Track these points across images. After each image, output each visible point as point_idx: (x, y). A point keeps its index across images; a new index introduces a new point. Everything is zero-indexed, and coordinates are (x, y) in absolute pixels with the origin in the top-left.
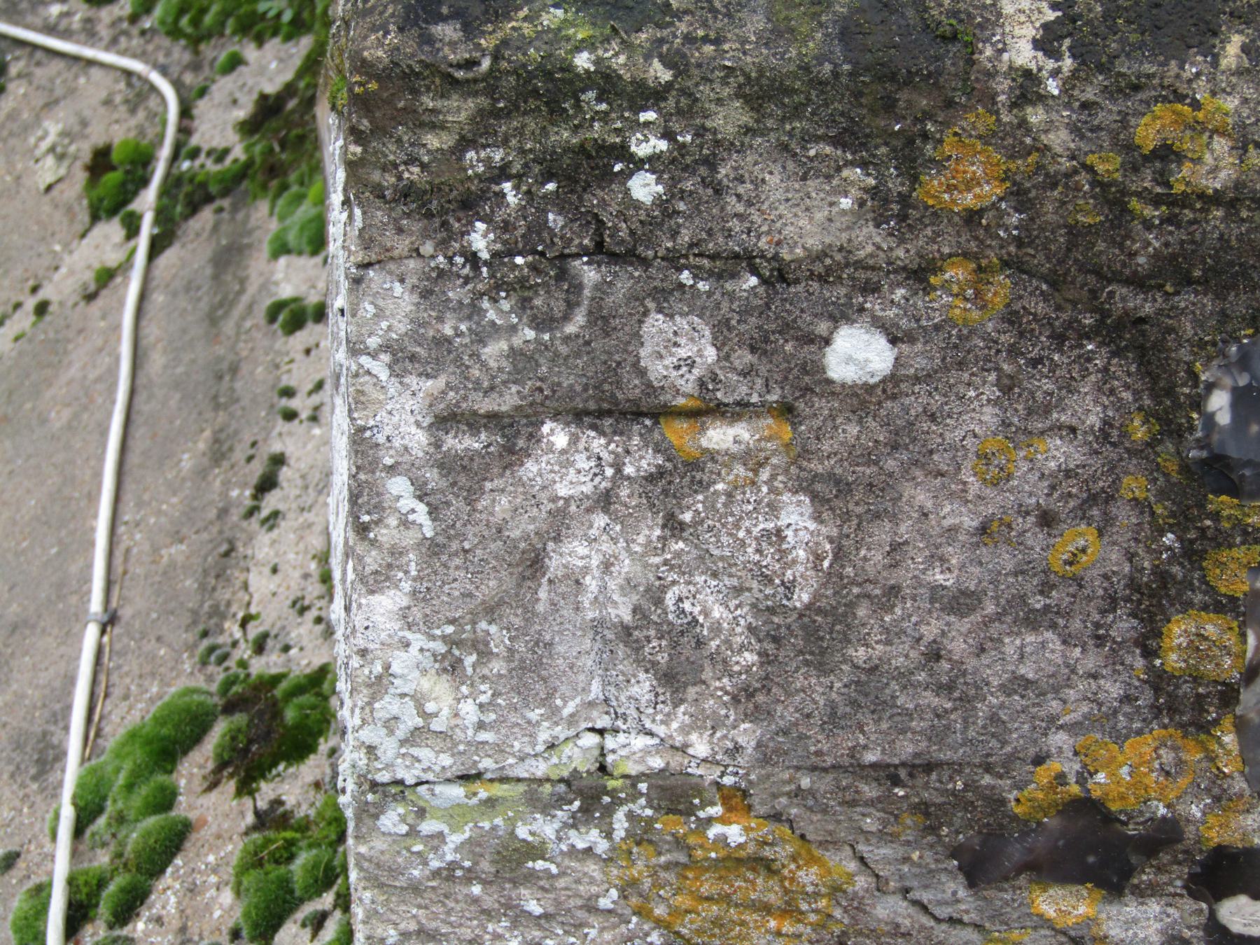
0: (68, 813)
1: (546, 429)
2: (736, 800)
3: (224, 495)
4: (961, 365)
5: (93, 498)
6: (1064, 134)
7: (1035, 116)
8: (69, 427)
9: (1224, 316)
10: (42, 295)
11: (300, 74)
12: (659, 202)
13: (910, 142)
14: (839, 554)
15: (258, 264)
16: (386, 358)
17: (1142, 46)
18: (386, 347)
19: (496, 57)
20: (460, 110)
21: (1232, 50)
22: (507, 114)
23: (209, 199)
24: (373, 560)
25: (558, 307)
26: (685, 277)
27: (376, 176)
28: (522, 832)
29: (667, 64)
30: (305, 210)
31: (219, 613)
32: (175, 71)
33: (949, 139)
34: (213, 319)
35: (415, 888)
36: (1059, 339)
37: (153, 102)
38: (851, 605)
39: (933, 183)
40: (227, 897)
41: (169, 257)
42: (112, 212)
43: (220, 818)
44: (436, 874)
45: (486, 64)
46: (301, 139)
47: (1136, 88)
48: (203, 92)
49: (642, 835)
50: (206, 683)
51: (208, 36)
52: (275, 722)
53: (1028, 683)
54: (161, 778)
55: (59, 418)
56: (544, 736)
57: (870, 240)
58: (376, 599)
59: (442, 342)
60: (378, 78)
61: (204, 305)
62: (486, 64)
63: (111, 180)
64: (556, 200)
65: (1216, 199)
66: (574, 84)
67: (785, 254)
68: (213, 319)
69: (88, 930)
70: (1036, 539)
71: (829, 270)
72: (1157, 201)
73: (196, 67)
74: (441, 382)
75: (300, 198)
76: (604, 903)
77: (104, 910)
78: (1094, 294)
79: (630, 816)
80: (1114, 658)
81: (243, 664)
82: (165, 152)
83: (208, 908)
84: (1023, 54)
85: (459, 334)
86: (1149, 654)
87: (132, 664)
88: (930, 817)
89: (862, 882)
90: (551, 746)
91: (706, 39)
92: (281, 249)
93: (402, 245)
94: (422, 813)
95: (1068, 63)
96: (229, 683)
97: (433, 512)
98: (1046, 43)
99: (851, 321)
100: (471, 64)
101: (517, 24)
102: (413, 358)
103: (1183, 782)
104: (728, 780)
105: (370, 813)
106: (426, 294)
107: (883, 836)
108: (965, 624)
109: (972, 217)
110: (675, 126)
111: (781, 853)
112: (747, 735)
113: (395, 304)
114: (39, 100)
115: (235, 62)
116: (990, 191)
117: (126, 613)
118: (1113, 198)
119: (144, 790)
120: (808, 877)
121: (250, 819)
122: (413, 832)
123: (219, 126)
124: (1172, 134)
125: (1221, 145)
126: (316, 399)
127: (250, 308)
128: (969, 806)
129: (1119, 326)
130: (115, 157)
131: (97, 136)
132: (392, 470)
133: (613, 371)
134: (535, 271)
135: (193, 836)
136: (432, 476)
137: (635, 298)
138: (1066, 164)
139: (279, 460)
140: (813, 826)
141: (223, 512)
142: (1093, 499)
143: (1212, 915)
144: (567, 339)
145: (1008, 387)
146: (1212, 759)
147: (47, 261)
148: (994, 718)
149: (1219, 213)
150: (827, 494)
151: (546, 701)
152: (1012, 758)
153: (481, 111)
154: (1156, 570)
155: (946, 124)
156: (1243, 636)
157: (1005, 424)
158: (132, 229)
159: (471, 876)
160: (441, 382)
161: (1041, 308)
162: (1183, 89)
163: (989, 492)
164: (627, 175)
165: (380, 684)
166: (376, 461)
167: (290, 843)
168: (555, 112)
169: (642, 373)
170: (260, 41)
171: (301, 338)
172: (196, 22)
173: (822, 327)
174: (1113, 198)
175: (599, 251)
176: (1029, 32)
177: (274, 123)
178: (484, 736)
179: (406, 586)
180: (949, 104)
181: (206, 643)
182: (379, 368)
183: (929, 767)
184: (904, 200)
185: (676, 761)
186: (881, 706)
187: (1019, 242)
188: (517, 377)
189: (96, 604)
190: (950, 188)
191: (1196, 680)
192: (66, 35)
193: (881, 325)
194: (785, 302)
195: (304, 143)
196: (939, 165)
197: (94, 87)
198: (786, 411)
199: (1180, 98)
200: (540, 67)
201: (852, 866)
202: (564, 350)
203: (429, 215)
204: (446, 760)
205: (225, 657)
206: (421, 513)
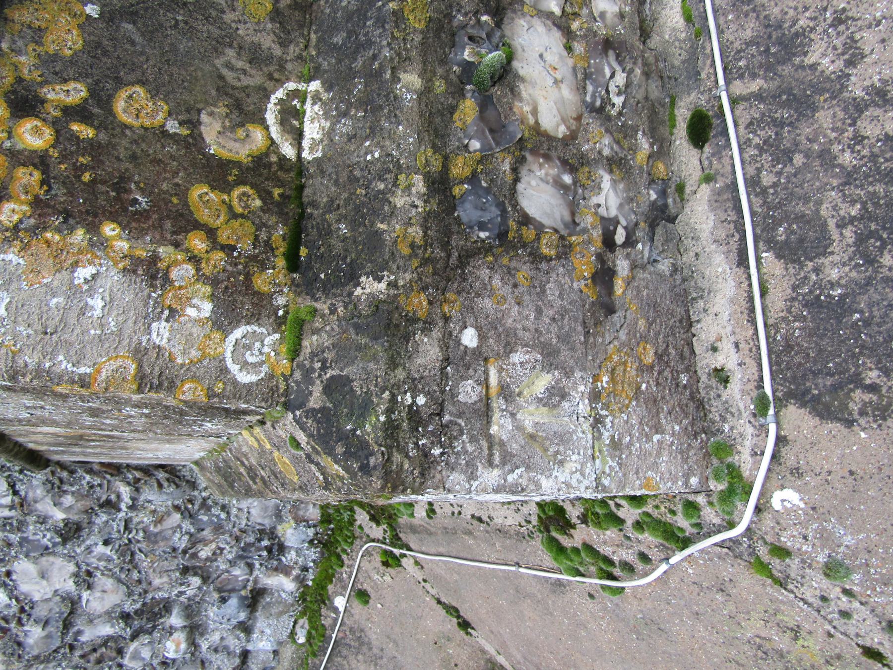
0: (578, 579)
1: (492, 432)
2: (596, 378)
3: (482, 531)
4: (472, 308)
5: (480, 568)
6: (406, 275)
7: (401, 283)
8: (459, 574)
9: (458, 232)
10: (421, 580)
11: (365, 510)
12: (425, 396)
13: (408, 320)
14: (527, 346)
15: (415, 521)
16: (472, 482)
17: (380, 252)
18: (469, 482)
19: (381, 445)
20: (397, 457)
21: (382, 226)
22: (398, 442)
23: (397, 534)
24: (532, 487)
25: (456, 428)
26: (448, 388)
27: (417, 484)
28: (607, 442)
29: (384, 392)
30: (402, 509)
31: (518, 533)
32: (362, 543)
33: (407, 308)
34: (431, 534)
35: (624, 475)
36: (465, 280)
37: (370, 549)
38: (541, 343)
39: (421, 314)
40: (608, 532)
41: (412, 546)
42: (399, 561)
43: (581, 534)
44: (620, 468)
45: (383, 449)
46: (382, 509)
47: (393, 254)
48: (368, 536)
49: (606, 406)
50: (539, 538)
51: (353, 534)
52: (553, 517)
53: (560, 293)
54: (569, 551)
55: (456, 577)
56: (581, 435)
57: (436, 333)
58: (543, 486)
59: (467, 464)
60: (387, 483)
61: (426, 536)
62: (383, 449)
63: (390, 561)
64: (425, 427)
65: (425, 232)
66: (389, 421)
67: (441, 358)
68: (431, 534)
69: (615, 573)
70: (521, 289)
71: (445, 346)
72: (426, 249)
73: (361, 538)
74: (479, 464)
75: (398, 510)
76: (625, 418)
77: (610, 569)
78: (452, 269)
79: (602, 410)
80: (553, 269)
81: (534, 527)
82: (384, 546)
83: (611, 538)
84: (382, 286)
85: (465, 459)
86: (551, 259)
87: (532, 559)
88: (598, 323)
89: (616, 343)
90: (583, 432)
91: (376, 381)
92: (412, 515)
93: (438, 476)
94: (604, 473)
95: (385, 273)
96: (540, 531)
97: (517, 468)
98: (379, 279)
99: (460, 340)
100: (383, 454)
101: (370, 439)
102: (472, 473)
103: (585, 252)
104: (591, 380)
105: (605, 489)
106: (453, 469)
107: (603, 337)
108: (545, 311)
109: (430, 303)
110: (403, 390)
111: (610, 365)
112: (578, 374)
113: (456, 478)
114: (369, 581)
115: (360, 527)
116: (423, 297)
117: (516, 560)
118: (425, 262)
119: (573, 556)
120: (615, 358)
121: (583, 526)
122: (609, 475)
123: (377, 531)
124: (406, 244)
125: (410, 230)
126: (455, 506)
127: (428, 524)
128: (594, 312)
129: (461, 262)
130: (385, 560)
131: (379, 565)
132: (505, 481)
133: (476, 411)
134: (445, 434)
135: (587, 542)
136: (507, 467)
137: (454, 404)
138: (415, 275)
139: (473, 516)
140: (601, 357)
141: (487, 532)
142: (509, 273)
143: (620, 246)
144: (466, 425)
145: (478, 295)
146: (579, 244)
147: (412, 579)
148: (570, 303)
149: (429, 232)
150: (509, 349)
151: (571, 434)
152: (581, 299)
153: (398, 451)
154: (529, 256)
155: (403, 309)
156: (546, 232)
157: (489, 296)
158: (404, 556)
159: (620, 458)
160: (479, 464)
161: (456, 284)
162: (393, 240)
163: (508, 302)
164: (417, 405)
165: (568, 485)
166: (503, 485)
167: (592, 514)
168: (398, 427)
169: (476, 402)
170: (355, 520)
171: (438, 510)
172: (349, 538)
173: (462, 348)
174: (425, 262)
175: (440, 415)
176: (376, 284)
177: (377, 517)
178: (582, 453)
179: (539, 476)
180: (397, 308)
181: (527, 538)
182: (475, 484)
183: (585, 323)
184: (425, 323)
185: (586, 396)
186: (568, 335)
187: (437, 290)
188: (477, 441)
189: (513, 568)
190: (422, 309)
191: (558, 246)
192: (351, 573)
193: (461, 331)
194: (455, 359)
195: (383, 509)
196: (415, 311)
197: (366, 565)
198: (486, 360)
199: (396, 241)
200: (384, 432)
201: (612, 346)
202: (469, 426)
203: (429, 467)
204: (589, 465)
205: (532, 532)
206: (518, 471)
